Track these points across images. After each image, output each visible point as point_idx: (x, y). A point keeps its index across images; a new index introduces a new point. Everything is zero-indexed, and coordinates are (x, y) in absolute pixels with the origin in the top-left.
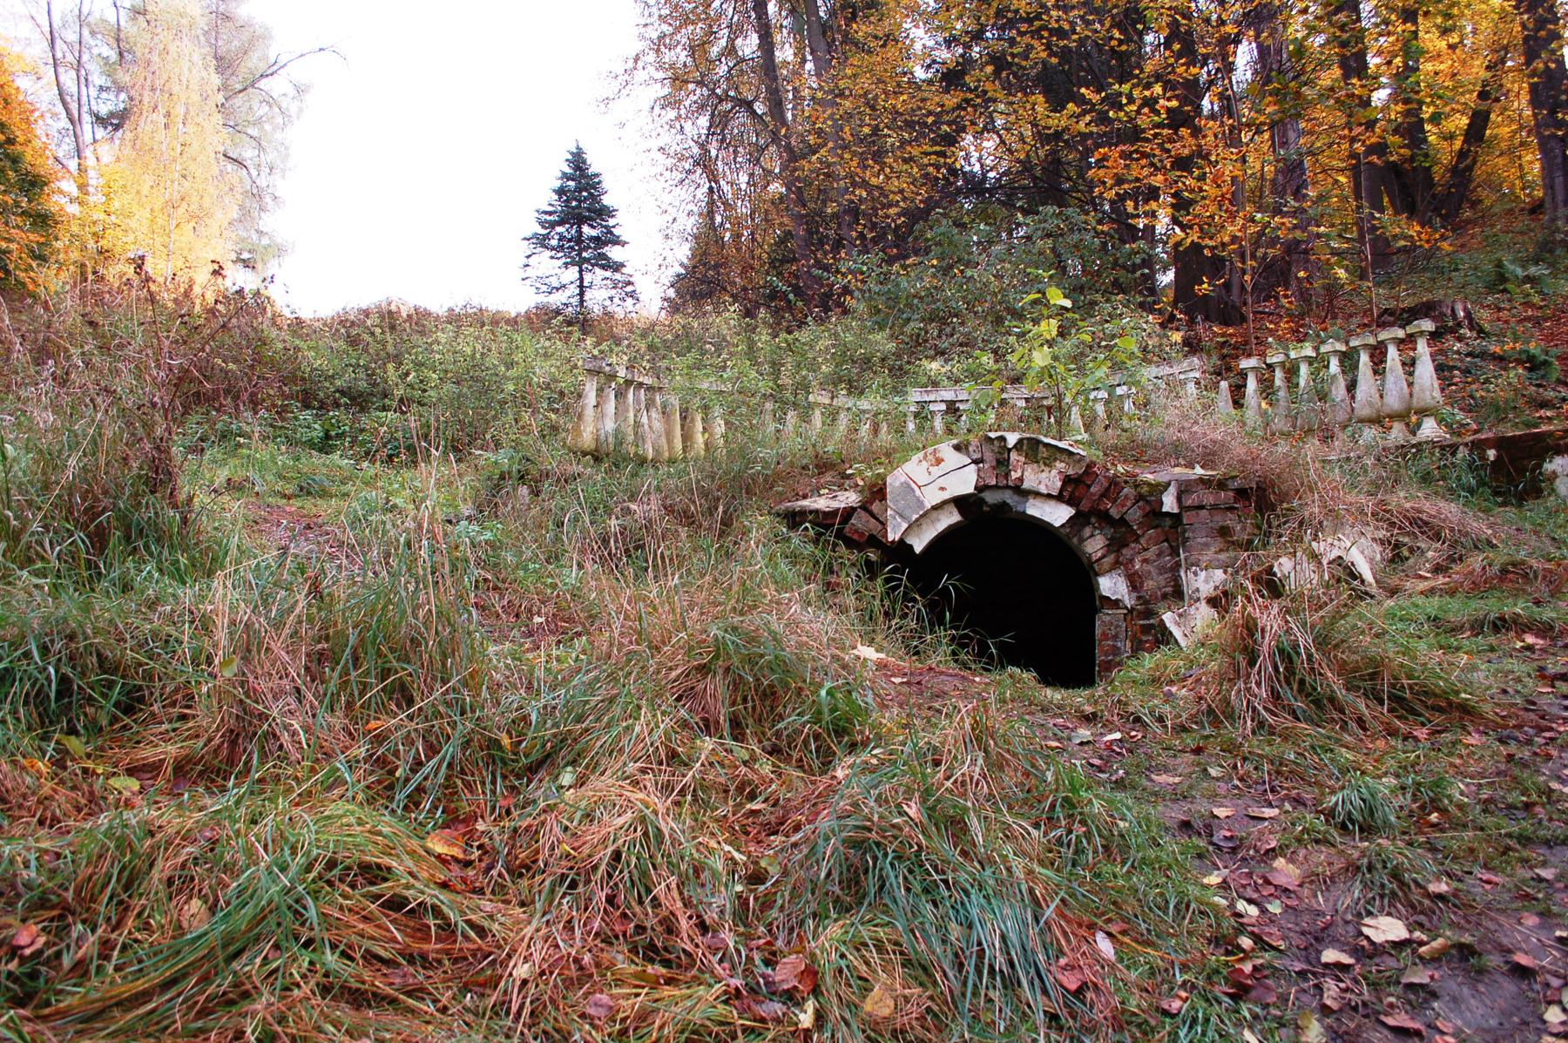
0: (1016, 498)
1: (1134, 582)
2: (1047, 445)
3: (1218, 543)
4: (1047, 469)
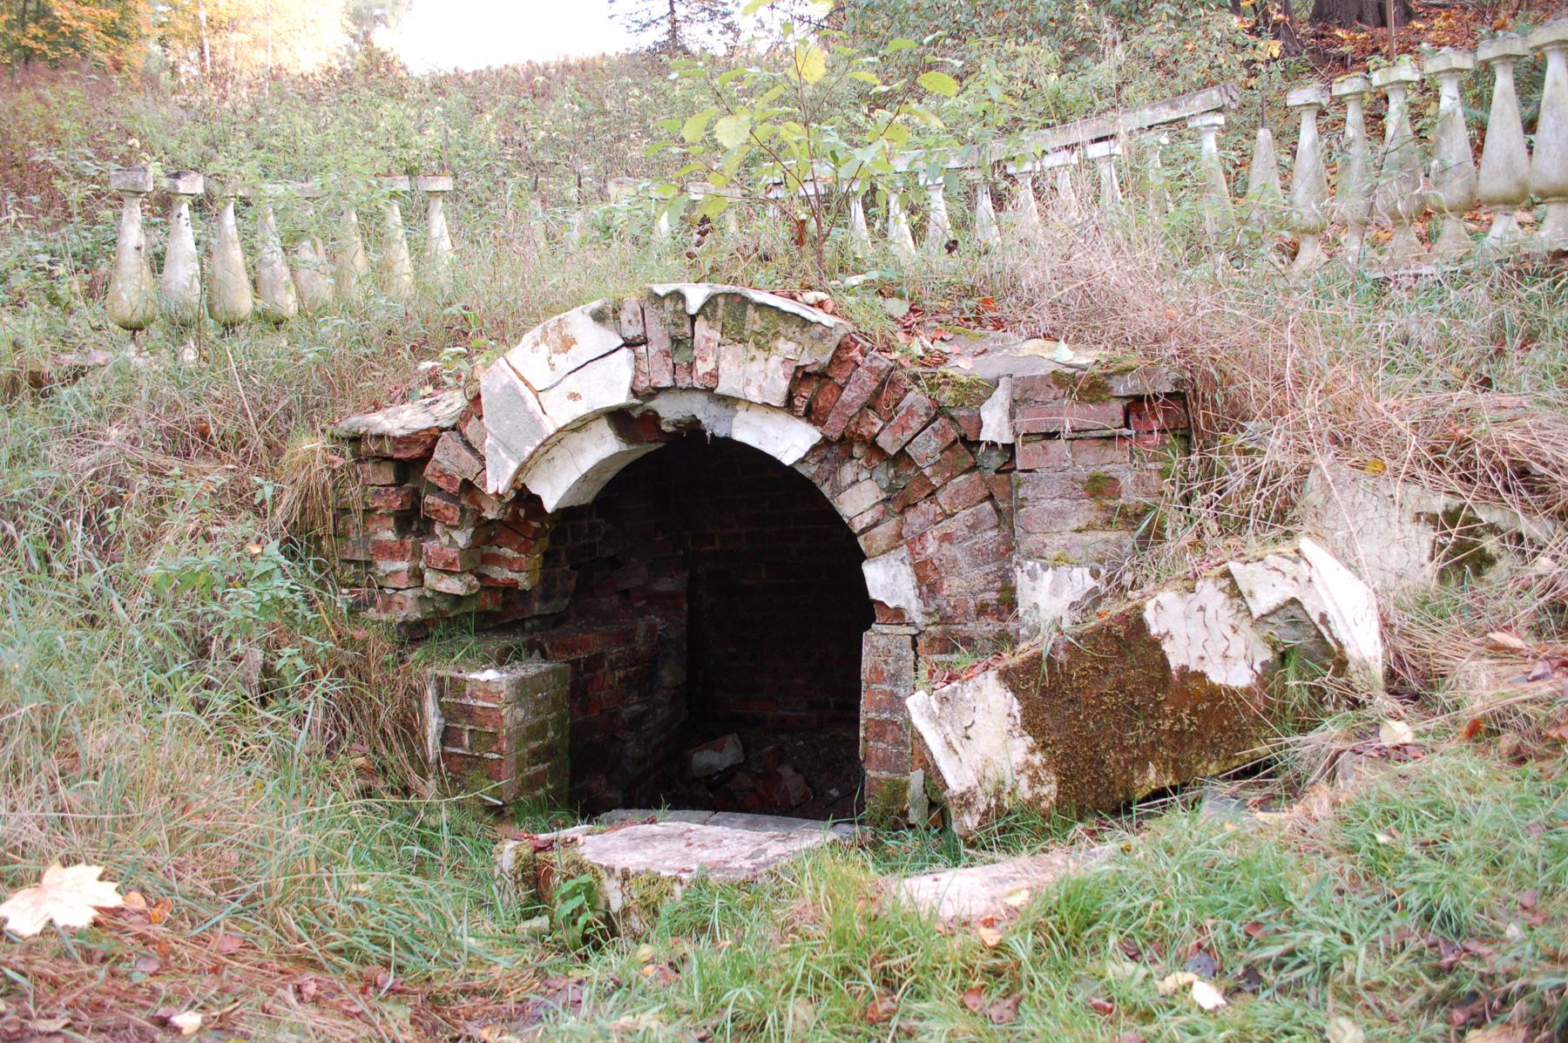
0: (713, 409)
1: (927, 579)
2: (761, 307)
3: (1086, 511)
4: (761, 355)
